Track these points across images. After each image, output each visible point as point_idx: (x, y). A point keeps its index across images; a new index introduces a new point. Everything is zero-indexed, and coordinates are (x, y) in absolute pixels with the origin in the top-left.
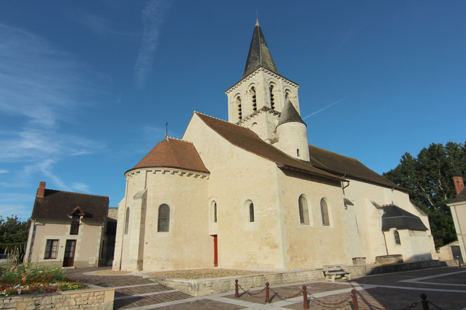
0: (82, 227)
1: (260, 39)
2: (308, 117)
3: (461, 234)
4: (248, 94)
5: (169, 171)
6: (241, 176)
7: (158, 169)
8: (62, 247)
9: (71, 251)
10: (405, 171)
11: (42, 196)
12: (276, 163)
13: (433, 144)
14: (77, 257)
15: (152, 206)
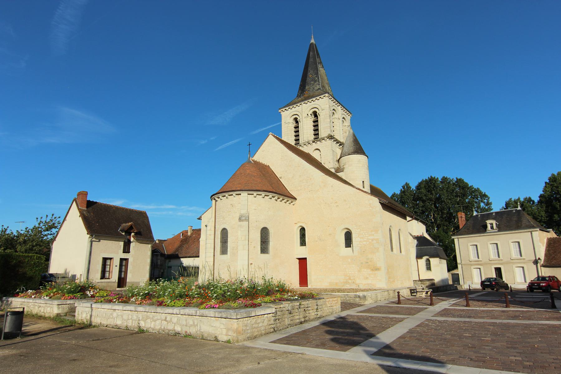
0: (134, 245)
1: (317, 59)
2: (275, 125)
3: (461, 263)
4: (309, 118)
5: (261, 195)
6: (337, 206)
7: (259, 193)
8: (116, 266)
9: (123, 271)
10: (403, 201)
11: (84, 207)
12: (378, 199)
13: (431, 177)
14: (130, 278)
15: (255, 229)
